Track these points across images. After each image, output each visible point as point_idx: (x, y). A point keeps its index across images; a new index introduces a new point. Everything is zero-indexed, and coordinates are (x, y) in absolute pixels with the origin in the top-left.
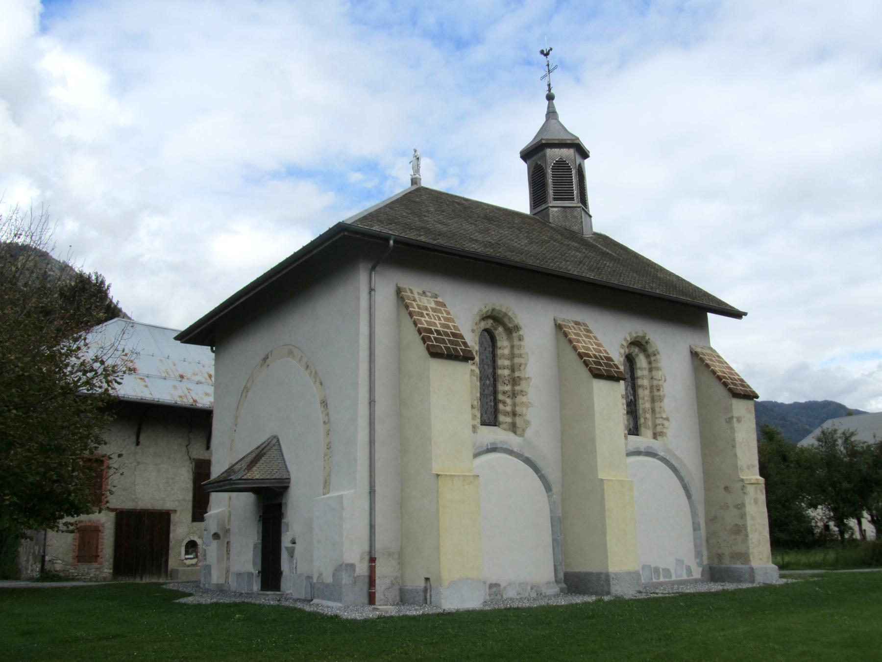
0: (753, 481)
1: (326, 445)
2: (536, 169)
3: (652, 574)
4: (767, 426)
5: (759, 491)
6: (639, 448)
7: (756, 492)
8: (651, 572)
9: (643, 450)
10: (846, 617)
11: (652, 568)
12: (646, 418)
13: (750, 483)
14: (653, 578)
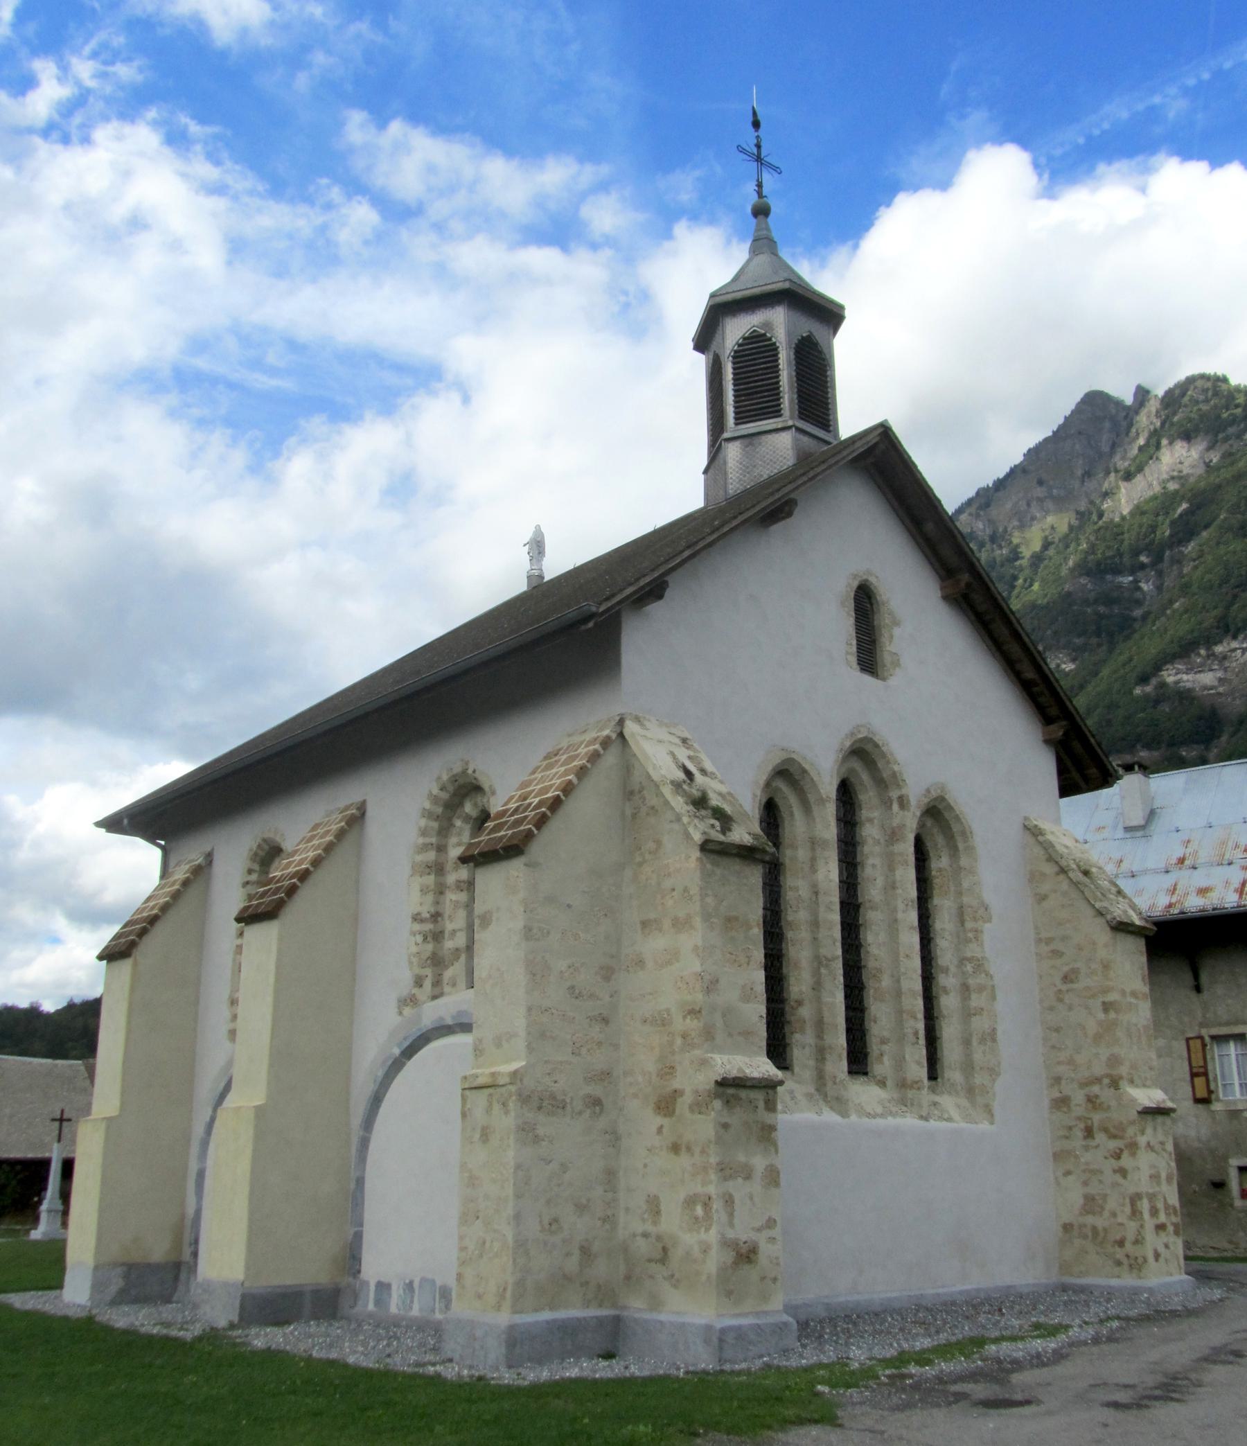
0: (481, 1081)
1: (1117, 1270)
2: (746, 341)
3: (434, 1300)
4: (875, 1022)
5: (496, 1108)
6: (441, 1019)
7: (489, 1110)
8: (435, 1296)
9: (449, 1022)
10: (457, 1369)
11: (438, 1287)
12: (950, 1050)
13: (473, 1086)
14: (437, 1311)
